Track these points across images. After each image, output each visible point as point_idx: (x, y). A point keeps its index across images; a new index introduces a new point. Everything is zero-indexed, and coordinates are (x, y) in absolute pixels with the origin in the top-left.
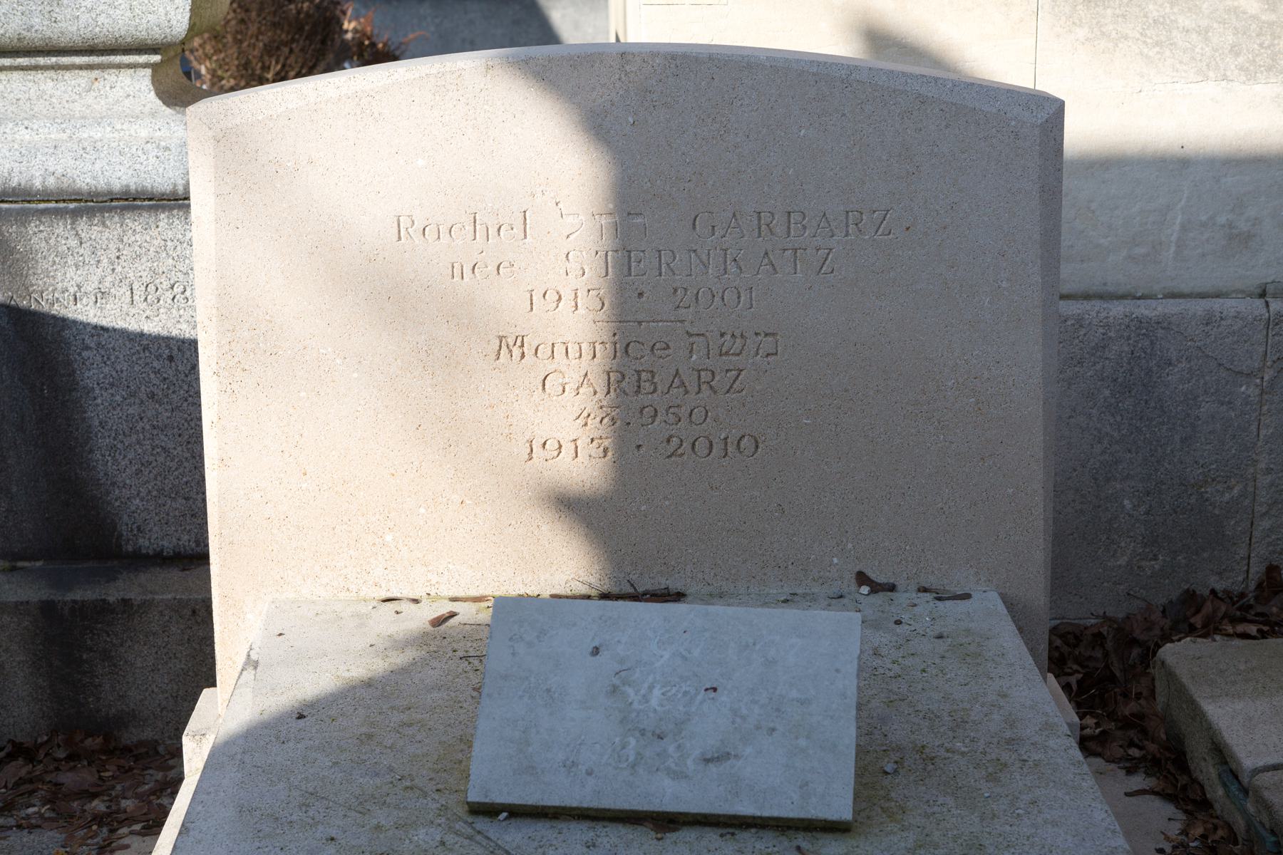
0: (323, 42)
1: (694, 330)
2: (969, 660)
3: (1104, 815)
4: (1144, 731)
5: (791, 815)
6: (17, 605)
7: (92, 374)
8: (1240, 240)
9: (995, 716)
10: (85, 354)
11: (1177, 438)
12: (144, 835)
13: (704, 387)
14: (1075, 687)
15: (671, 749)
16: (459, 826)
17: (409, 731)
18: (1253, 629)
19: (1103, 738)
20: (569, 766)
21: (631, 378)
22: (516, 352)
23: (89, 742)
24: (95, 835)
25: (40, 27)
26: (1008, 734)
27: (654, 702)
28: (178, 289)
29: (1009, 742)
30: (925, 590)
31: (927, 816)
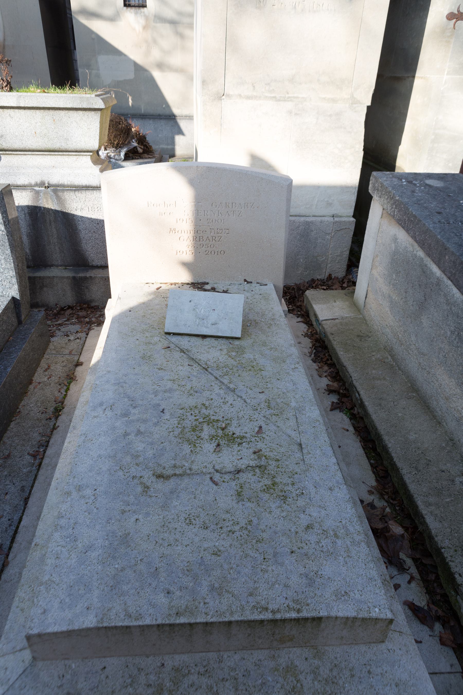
0: (128, 134)
1: (212, 228)
2: (266, 300)
3: (290, 336)
4: (301, 309)
5: (229, 336)
6: (67, 277)
7: (81, 227)
8: (329, 204)
9: (270, 313)
10: (79, 222)
11: (313, 247)
12: (97, 326)
13: (213, 240)
14: (288, 299)
15: (205, 322)
16: (163, 337)
17: (152, 315)
18: (325, 288)
19: (293, 310)
20: (185, 325)
21: (198, 237)
22: (174, 232)
23: (84, 306)
24: (87, 326)
25: (64, 146)
26: (273, 318)
27: (202, 312)
28: (99, 208)
29: (273, 319)
30: (258, 283)
31: (255, 336)
